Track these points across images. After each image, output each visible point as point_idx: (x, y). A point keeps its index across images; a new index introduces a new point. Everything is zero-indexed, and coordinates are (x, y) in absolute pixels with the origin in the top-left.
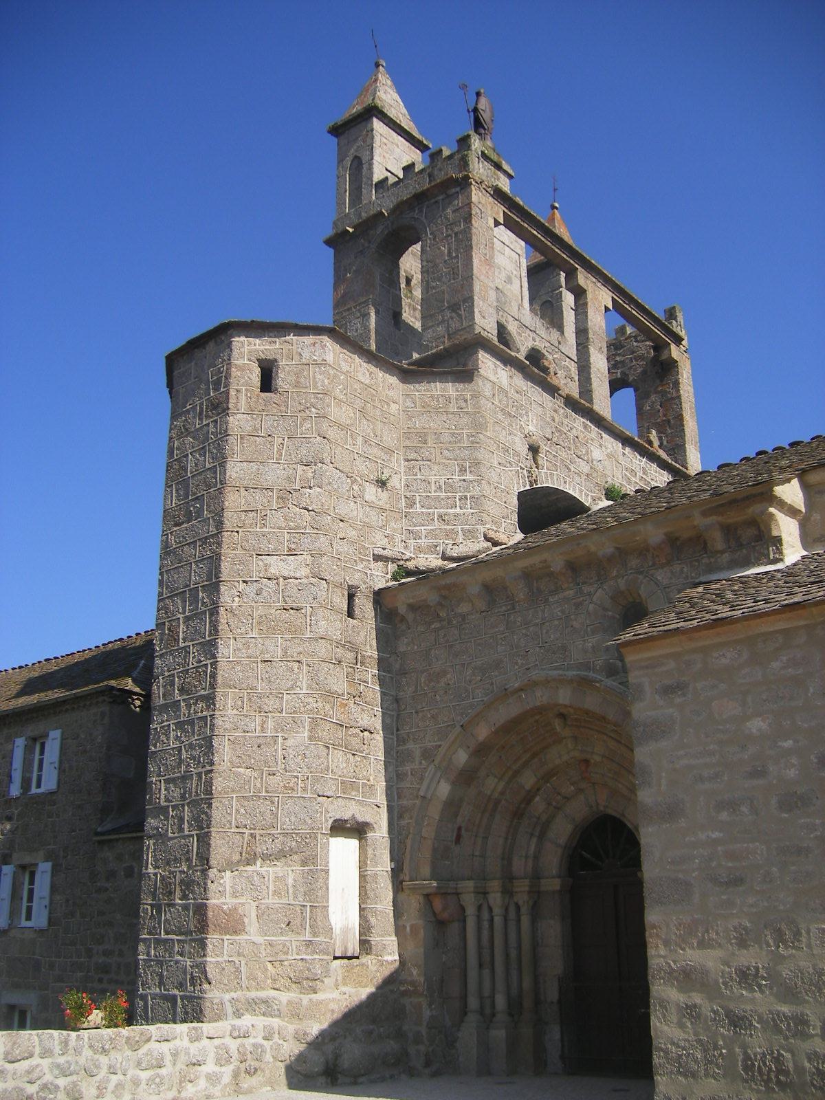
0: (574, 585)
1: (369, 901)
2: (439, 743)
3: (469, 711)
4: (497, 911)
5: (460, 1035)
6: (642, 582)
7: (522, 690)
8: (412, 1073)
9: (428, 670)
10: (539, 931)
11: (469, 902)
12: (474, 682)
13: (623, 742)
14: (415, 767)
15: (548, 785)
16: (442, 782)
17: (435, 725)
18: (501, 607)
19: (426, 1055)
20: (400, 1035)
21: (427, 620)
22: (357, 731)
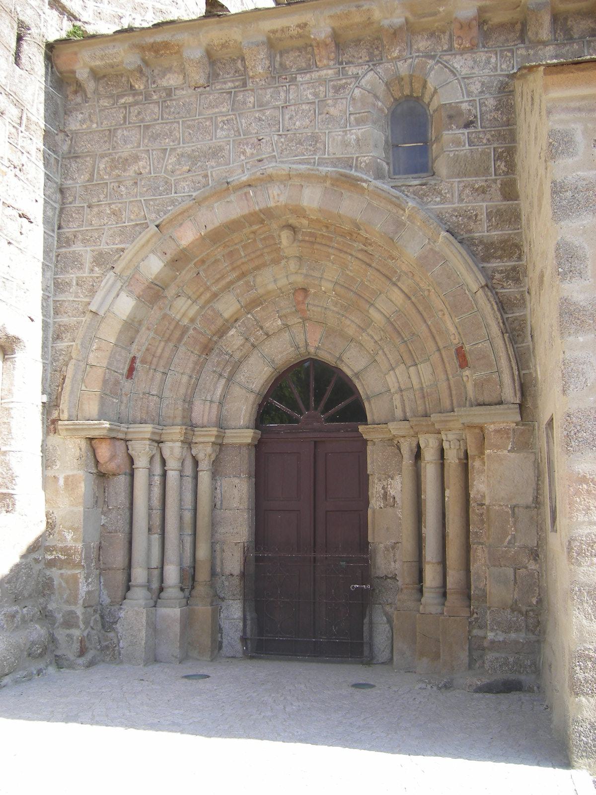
0: (335, 64)
1: (13, 442)
2: (122, 246)
3: (170, 208)
4: (172, 464)
5: (122, 614)
6: (432, 69)
7: (250, 185)
8: (60, 663)
9: (110, 154)
10: (218, 491)
11: (142, 452)
12: (178, 172)
13: (373, 265)
14: (84, 275)
15: (249, 316)
16: (123, 295)
17: (117, 223)
18: (225, 83)
19: (81, 642)
20: (46, 616)
21: (114, 92)
22: (15, 213)
